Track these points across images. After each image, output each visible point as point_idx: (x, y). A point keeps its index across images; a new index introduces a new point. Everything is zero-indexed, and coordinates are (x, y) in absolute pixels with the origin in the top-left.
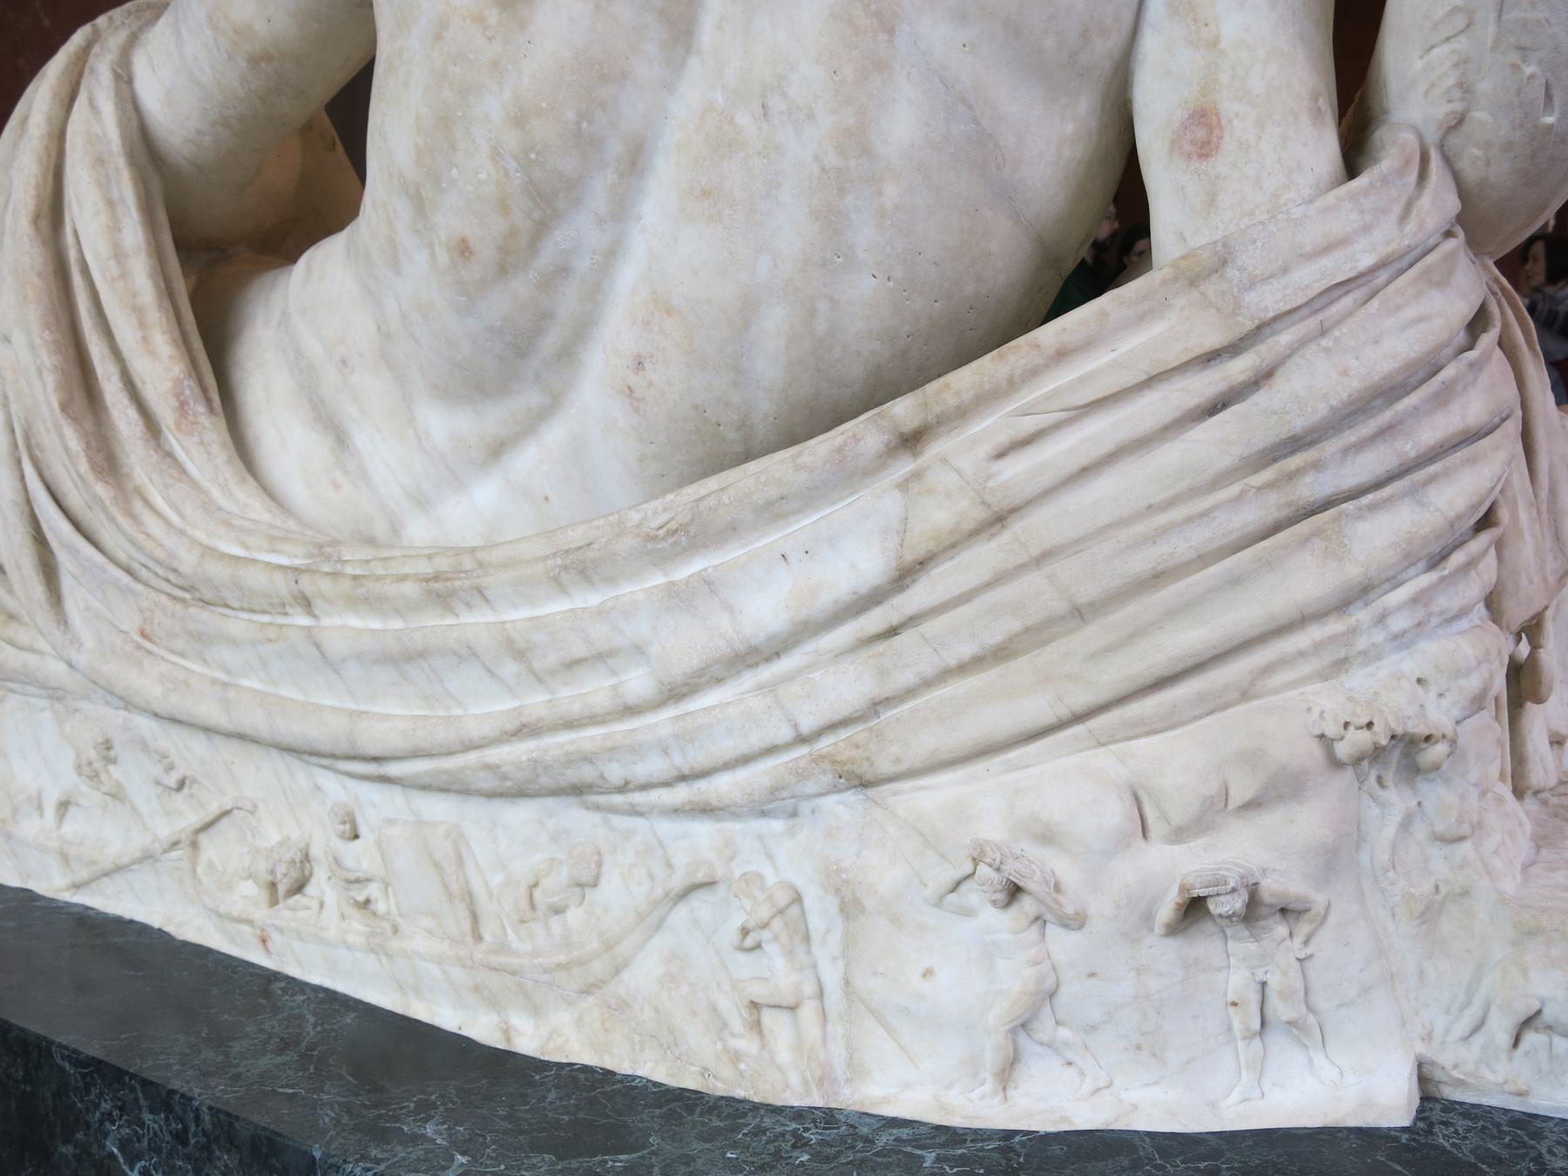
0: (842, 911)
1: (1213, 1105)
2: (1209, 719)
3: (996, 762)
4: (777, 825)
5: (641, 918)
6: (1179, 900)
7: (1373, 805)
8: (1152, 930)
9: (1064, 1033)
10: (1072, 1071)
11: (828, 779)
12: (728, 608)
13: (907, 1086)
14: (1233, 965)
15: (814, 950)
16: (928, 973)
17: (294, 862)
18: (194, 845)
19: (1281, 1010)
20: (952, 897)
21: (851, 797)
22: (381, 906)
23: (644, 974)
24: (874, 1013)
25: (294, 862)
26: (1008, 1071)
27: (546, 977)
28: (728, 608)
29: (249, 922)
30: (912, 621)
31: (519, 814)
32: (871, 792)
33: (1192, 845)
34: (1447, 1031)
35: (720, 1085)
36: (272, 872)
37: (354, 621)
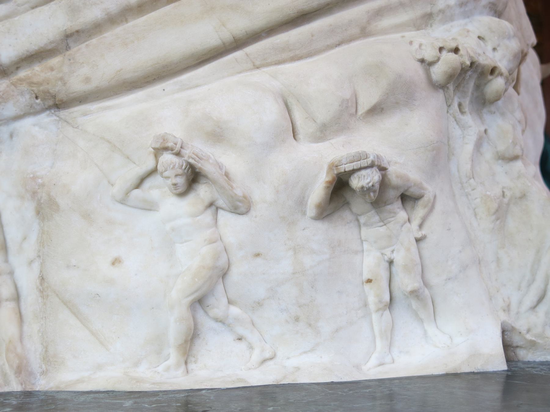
0: (38, 213)
1: (358, 367)
2: (337, 49)
3: (170, 84)
6: (329, 178)
7: (457, 127)
8: (304, 213)
9: (234, 310)
10: (242, 346)
11: (25, 100)
13: (100, 367)
14: (371, 245)
15: (11, 258)
16: (116, 262)
19: (406, 282)
20: (136, 191)
21: (45, 118)
24: (67, 304)
26: (190, 342)
32: (64, 113)
33: (333, 141)
34: (520, 303)
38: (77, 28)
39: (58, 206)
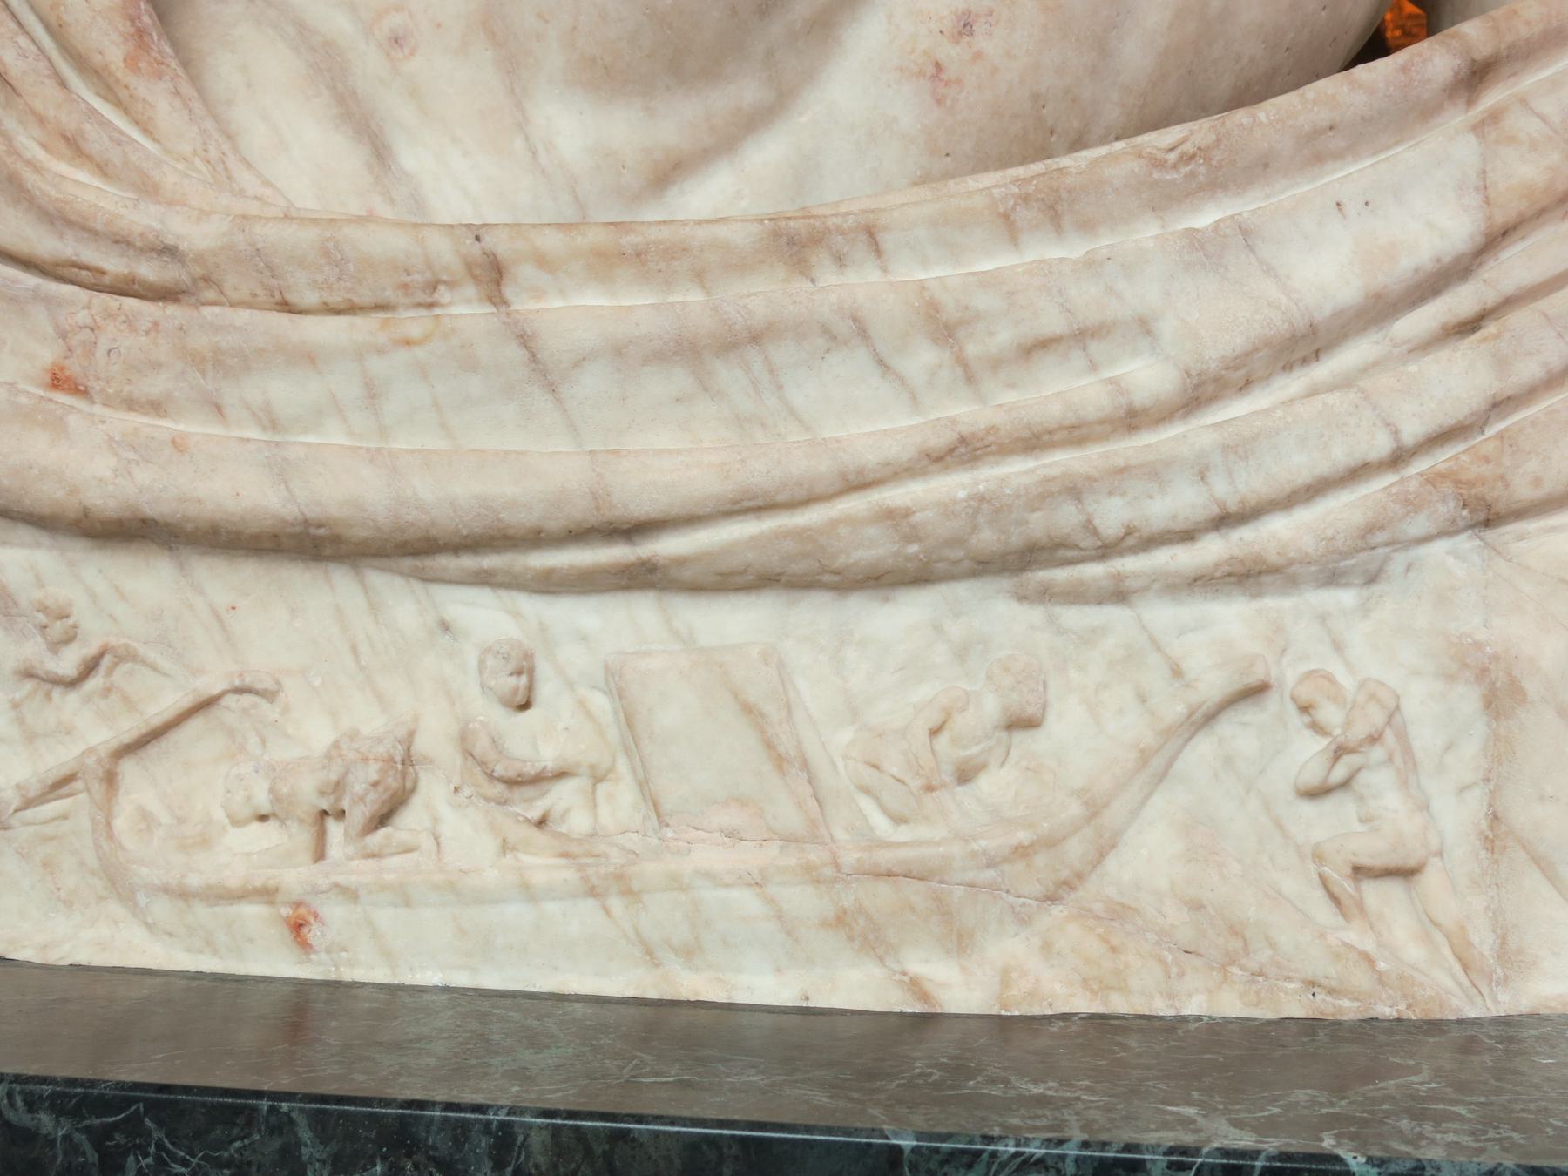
4: (1346, 597)
5: (1145, 757)
11: (1446, 509)
12: (1269, 270)
17: (391, 760)
18: (110, 779)
22: (579, 822)
23: (1149, 857)
25: (391, 760)
27: (989, 875)
28: (1269, 270)
29: (267, 894)
30: (1509, 303)
31: (900, 618)
32: (1491, 535)
35: (1345, 1003)
36: (338, 787)
37: (593, 298)
38: (1509, 392)
39: (1525, 695)
